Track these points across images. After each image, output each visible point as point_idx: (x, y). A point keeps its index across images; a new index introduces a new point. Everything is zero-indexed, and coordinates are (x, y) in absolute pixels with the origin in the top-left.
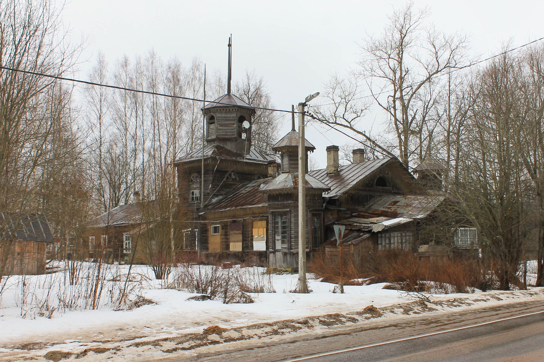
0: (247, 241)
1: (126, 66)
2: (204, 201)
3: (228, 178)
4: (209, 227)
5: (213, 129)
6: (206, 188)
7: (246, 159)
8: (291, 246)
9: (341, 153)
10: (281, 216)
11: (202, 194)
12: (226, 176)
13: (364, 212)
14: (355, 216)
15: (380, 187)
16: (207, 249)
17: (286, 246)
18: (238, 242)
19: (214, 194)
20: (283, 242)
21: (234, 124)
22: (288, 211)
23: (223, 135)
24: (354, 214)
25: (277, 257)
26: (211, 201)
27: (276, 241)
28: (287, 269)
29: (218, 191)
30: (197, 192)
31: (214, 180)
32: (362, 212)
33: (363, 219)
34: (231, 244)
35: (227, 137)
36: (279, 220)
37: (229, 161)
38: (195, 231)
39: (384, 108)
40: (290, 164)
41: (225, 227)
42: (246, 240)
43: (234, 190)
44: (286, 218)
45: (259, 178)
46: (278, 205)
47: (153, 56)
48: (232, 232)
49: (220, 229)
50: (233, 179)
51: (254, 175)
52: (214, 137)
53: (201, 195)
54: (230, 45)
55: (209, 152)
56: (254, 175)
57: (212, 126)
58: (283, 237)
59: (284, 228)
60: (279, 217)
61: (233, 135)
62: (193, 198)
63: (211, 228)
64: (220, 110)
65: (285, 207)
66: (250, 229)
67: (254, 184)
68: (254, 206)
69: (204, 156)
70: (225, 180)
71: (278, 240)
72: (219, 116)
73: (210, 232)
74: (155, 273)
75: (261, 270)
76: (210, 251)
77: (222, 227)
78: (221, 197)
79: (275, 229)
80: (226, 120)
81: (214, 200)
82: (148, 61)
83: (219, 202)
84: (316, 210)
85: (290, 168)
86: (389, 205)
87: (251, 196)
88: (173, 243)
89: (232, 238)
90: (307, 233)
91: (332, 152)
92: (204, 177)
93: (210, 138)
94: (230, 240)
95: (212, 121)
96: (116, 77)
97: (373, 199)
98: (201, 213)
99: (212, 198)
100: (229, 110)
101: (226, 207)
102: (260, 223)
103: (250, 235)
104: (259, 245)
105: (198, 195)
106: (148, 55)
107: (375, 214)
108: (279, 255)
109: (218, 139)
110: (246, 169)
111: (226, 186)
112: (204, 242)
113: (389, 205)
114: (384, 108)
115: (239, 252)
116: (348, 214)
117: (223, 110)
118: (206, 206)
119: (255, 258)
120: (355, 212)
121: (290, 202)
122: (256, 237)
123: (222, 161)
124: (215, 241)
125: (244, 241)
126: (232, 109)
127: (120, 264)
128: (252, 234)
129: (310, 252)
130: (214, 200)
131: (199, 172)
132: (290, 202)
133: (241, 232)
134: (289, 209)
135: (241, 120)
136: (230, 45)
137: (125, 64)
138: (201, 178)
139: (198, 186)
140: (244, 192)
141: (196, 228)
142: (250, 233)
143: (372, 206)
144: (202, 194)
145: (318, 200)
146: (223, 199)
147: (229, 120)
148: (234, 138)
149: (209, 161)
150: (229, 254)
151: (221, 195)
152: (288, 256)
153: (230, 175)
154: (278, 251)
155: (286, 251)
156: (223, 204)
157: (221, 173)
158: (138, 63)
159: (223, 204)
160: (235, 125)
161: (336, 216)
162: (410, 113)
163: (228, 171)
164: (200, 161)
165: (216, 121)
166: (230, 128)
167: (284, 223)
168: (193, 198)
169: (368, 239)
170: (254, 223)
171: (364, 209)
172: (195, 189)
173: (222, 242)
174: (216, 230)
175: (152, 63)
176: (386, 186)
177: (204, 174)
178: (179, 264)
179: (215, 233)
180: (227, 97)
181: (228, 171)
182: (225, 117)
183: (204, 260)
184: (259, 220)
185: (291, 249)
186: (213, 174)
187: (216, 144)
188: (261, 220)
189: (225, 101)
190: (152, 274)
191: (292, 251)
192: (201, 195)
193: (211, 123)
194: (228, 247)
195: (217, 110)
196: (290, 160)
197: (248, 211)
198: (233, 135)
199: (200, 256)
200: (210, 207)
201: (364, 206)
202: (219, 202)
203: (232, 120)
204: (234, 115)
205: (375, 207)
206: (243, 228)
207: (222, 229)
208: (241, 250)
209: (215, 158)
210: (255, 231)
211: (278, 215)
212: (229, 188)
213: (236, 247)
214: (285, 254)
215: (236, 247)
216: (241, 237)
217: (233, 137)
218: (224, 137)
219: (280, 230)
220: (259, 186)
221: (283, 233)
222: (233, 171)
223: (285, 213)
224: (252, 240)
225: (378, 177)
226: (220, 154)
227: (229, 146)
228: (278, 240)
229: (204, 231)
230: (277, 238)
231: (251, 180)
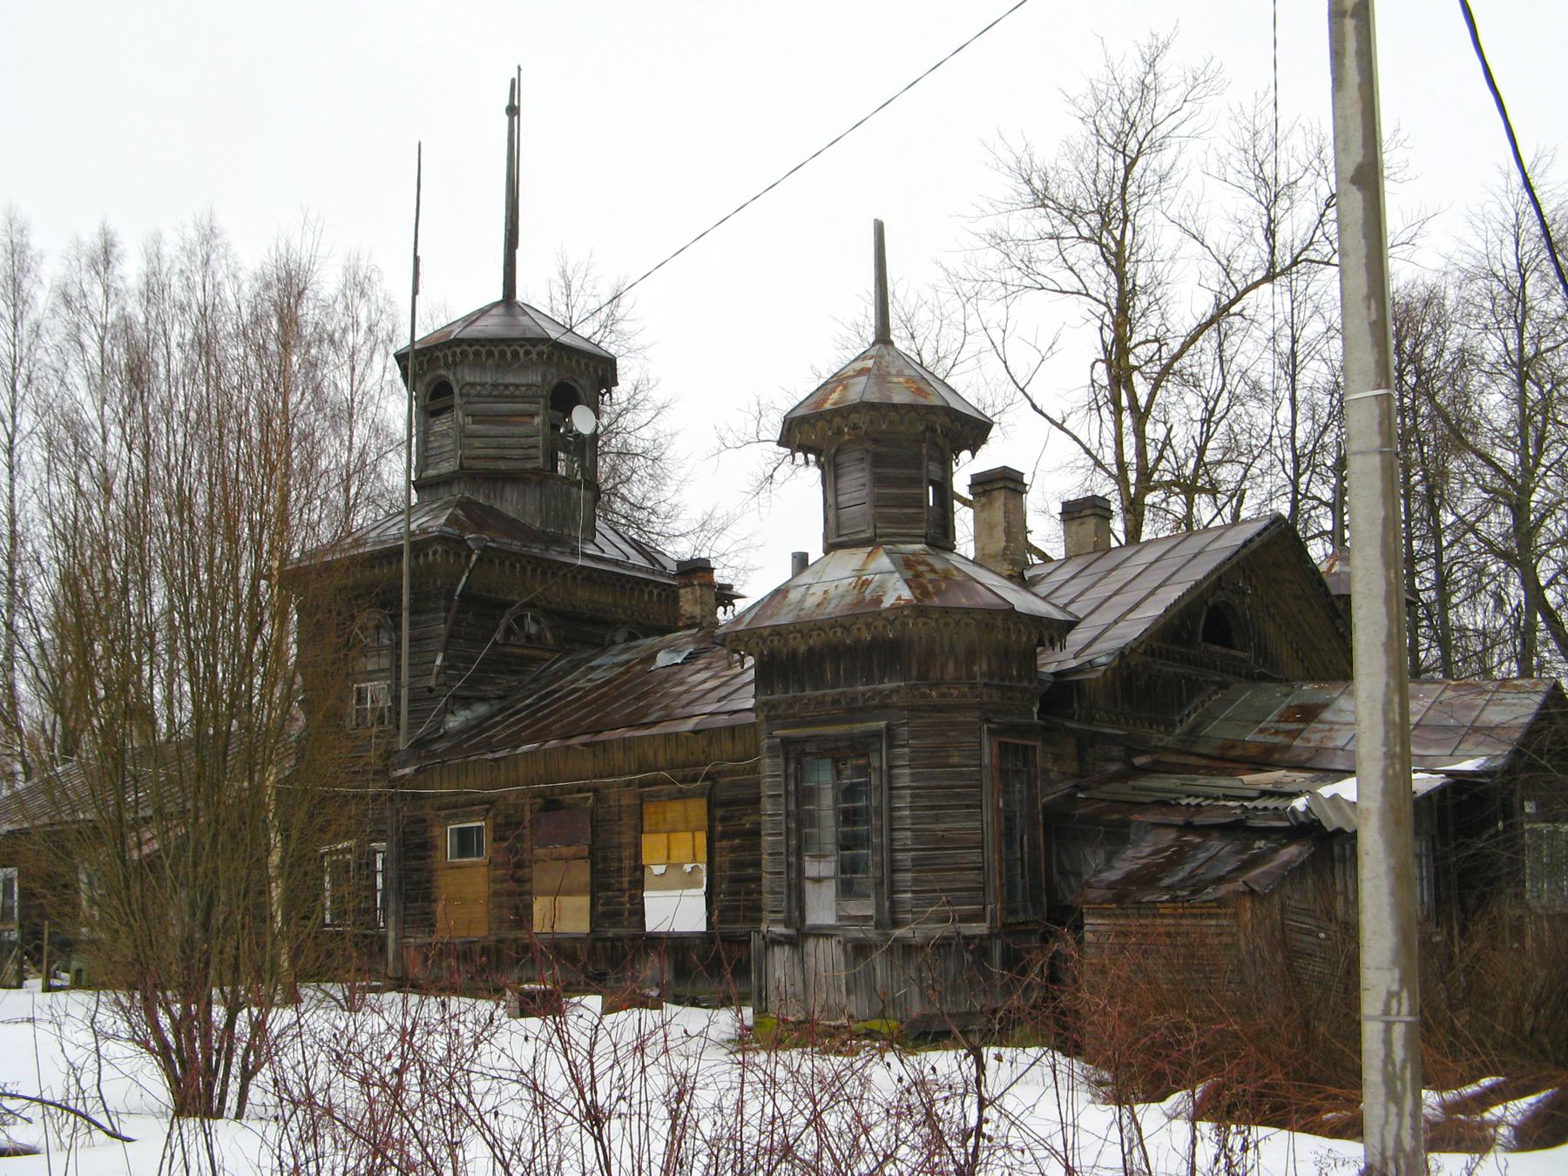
0: (617, 890)
1: (107, 263)
2: (412, 726)
3: (509, 631)
4: (436, 831)
5: (444, 435)
6: (420, 667)
7: (585, 555)
8: (893, 911)
9: (1032, 501)
10: (837, 761)
11: (404, 692)
12: (503, 623)
13: (1180, 752)
14: (1146, 771)
15: (1218, 648)
16: (427, 921)
17: (864, 908)
18: (570, 892)
19: (454, 697)
20: (847, 890)
21: (532, 415)
22: (877, 735)
23: (487, 458)
24: (1140, 761)
25: (811, 961)
26: (442, 723)
27: (809, 887)
28: (875, 1025)
29: (472, 683)
30: (376, 690)
31: (451, 635)
32: (1165, 750)
33: (1203, 780)
34: (540, 906)
35: (502, 465)
36: (824, 779)
37: (517, 556)
38: (375, 852)
39: (1052, 421)
40: (879, 502)
41: (507, 828)
42: (609, 887)
43: (535, 680)
44: (863, 771)
45: (632, 637)
46: (820, 702)
47: (209, 236)
48: (540, 852)
49: (486, 838)
50: (529, 637)
51: (610, 624)
52: (446, 467)
53: (396, 699)
54: (513, 111)
55: (431, 521)
56: (610, 624)
57: (441, 425)
58: (848, 868)
59: (848, 817)
60: (827, 764)
61: (530, 458)
62: (361, 714)
63: (447, 836)
64: (477, 354)
65: (856, 711)
66: (627, 838)
67: (624, 657)
68: (655, 730)
69: (412, 534)
70: (498, 636)
71: (818, 880)
72: (469, 378)
73: (439, 855)
74: (168, 1067)
75: (724, 1022)
76: (441, 936)
77: (496, 827)
78: (482, 709)
79: (800, 825)
80: (502, 398)
81: (454, 722)
82: (191, 254)
83: (479, 726)
84: (1012, 729)
85: (878, 517)
86: (1284, 718)
87: (624, 695)
88: (276, 892)
89: (544, 876)
90: (1398, 822)
91: (1000, 499)
92: (412, 625)
93: (431, 472)
94: (536, 887)
95: (440, 403)
96: (68, 302)
97: (1196, 701)
98: (401, 772)
99: (447, 711)
100: (515, 354)
101: (515, 741)
102: (675, 810)
103: (627, 864)
104: (676, 910)
105: (385, 702)
106: (192, 234)
107: (1234, 760)
108: (826, 956)
109: (467, 474)
110: (583, 596)
111: (502, 664)
112: (415, 890)
113: (1284, 718)
114: (1052, 421)
115: (576, 939)
116: (1113, 760)
117: (490, 354)
118: (420, 744)
119: (652, 968)
120: (1142, 753)
121: (888, 685)
122: (658, 870)
123: (487, 555)
124: (465, 892)
125: (597, 888)
126: (527, 353)
127: (48, 988)
128: (638, 855)
129: (990, 936)
130: (454, 722)
131: (389, 601)
132: (888, 685)
133: (584, 849)
134: (883, 724)
135: (563, 399)
136: (513, 111)
137: (105, 257)
138: (397, 627)
139: (385, 663)
140: (581, 684)
141: (380, 835)
142: (626, 853)
143: (1196, 727)
144: (404, 692)
145: (1020, 678)
146: (493, 716)
147: (512, 398)
148: (536, 470)
149: (435, 554)
150: (526, 948)
151: (483, 700)
152: (877, 958)
153: (520, 620)
154: (822, 933)
155: (871, 933)
156: (500, 733)
157: (481, 607)
158: (154, 257)
159: (500, 733)
160: (537, 420)
161: (1073, 767)
162: (1154, 431)
163: (510, 604)
164: (390, 555)
165: (457, 400)
166: (516, 430)
167: (850, 793)
168: (361, 714)
169: (1295, 873)
170: (650, 809)
171: (1169, 741)
172: (370, 676)
173: (495, 894)
174: (466, 843)
175: (206, 263)
176: (1231, 646)
177: (413, 612)
178: (307, 991)
179: (461, 855)
180: (500, 310)
181: (510, 604)
182: (495, 386)
183: (417, 971)
184: (672, 797)
185: (896, 924)
186: (448, 610)
187: (459, 491)
188: (682, 796)
189: (490, 326)
190: (136, 1081)
191: (898, 932)
192: (396, 699)
193: (436, 413)
194: (523, 916)
195: (464, 354)
196: (878, 481)
197: (619, 757)
198: (530, 458)
199: (399, 956)
200: (440, 747)
201: (1170, 726)
202: (478, 725)
203: (525, 399)
204: (534, 377)
205: (1219, 731)
206: (594, 834)
207: (498, 838)
208: (583, 927)
209: (461, 541)
210: (653, 849)
211: (821, 755)
212: (514, 673)
213: (565, 914)
214: (860, 950)
215: (565, 914)
216: (582, 873)
217: (529, 465)
218: (491, 465)
219: (828, 830)
220: (652, 658)
221: (847, 842)
222: (530, 605)
223: (861, 746)
224: (639, 885)
225: (1210, 602)
226: (480, 526)
227: (511, 503)
228: (818, 880)
229: (414, 851)
230: (812, 868)
231: (603, 646)
